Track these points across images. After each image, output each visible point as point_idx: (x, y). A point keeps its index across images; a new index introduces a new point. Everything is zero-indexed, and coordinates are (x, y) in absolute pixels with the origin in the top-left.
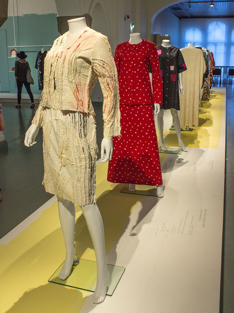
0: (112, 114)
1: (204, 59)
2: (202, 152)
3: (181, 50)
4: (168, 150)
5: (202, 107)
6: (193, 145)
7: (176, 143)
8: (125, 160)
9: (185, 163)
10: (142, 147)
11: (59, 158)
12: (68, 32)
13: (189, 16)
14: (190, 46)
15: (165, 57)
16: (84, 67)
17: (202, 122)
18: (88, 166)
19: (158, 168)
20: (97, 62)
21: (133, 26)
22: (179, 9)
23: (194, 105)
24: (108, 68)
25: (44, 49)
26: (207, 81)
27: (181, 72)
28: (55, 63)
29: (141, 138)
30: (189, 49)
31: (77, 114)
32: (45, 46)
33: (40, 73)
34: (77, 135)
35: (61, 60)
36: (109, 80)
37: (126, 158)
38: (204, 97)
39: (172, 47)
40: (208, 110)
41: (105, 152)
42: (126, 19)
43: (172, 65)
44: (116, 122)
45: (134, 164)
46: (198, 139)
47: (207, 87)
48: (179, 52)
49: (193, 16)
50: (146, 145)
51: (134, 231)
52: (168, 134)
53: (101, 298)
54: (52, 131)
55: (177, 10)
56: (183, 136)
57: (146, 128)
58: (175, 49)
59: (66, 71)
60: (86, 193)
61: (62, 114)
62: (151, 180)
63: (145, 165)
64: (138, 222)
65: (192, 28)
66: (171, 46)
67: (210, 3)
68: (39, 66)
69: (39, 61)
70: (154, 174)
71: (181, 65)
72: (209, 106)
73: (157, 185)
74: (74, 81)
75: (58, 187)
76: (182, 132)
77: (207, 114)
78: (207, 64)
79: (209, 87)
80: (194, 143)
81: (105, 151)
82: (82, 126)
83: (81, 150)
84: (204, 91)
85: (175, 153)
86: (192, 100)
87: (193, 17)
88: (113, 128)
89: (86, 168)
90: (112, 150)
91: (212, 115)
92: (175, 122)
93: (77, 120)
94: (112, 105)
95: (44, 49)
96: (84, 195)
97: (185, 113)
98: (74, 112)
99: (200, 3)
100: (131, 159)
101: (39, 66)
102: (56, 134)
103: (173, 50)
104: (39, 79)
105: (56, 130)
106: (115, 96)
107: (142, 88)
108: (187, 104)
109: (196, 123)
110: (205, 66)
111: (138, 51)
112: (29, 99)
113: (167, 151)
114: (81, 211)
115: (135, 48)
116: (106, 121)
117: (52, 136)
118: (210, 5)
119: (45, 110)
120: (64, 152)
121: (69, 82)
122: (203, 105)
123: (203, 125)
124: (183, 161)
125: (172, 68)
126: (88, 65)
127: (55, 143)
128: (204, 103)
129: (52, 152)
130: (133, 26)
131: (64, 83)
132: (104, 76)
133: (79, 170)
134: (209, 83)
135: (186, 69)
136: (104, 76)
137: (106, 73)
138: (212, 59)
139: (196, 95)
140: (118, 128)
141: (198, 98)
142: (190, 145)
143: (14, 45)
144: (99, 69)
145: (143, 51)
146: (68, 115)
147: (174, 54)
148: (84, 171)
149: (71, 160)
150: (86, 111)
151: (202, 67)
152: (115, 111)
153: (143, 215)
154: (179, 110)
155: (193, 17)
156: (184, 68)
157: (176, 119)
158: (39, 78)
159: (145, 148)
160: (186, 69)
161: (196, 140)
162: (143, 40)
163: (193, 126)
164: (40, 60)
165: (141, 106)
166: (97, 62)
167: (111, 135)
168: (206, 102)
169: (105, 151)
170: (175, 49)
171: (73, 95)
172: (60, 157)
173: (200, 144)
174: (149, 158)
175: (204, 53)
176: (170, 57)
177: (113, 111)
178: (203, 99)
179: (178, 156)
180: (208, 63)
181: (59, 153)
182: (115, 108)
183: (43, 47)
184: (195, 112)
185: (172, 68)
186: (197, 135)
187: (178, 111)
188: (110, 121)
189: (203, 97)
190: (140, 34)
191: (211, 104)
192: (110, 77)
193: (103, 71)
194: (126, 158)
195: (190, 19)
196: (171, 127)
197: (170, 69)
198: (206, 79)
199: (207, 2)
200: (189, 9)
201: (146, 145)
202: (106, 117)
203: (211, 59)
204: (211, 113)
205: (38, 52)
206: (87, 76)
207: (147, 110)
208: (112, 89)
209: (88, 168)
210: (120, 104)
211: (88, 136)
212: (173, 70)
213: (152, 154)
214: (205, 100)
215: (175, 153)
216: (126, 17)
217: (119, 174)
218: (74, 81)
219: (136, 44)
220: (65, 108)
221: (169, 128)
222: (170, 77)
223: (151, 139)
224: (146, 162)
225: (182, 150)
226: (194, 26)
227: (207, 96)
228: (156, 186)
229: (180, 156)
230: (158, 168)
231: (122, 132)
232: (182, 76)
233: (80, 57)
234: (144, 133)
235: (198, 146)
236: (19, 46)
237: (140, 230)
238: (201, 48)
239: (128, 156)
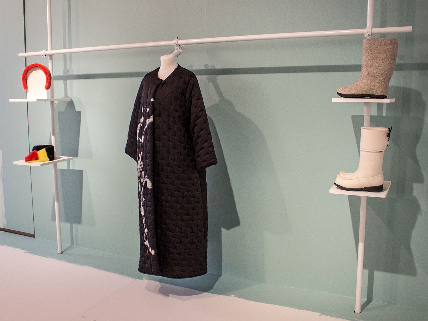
25: (171, 56)
32: (181, 42)
33: (149, 185)
68: (142, 147)
69: (145, 122)
95: (171, 56)
101: (142, 147)
104: (141, 217)
112: (198, 75)
119: (212, 65)
143: (364, 26)
158: (143, 213)
164: (147, 116)
183: (167, 50)
205: (141, 79)
236: (70, 47)
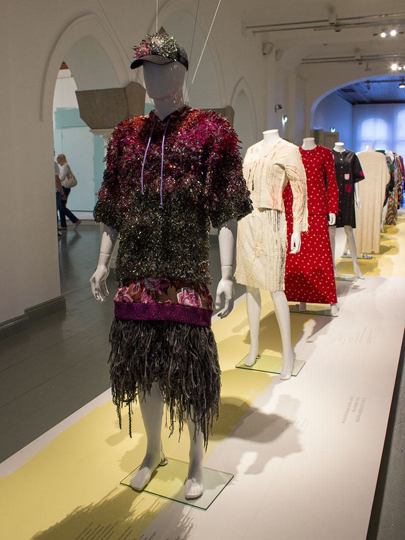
0: (301, 212)
1: (388, 165)
2: (384, 280)
3: (357, 154)
4: (341, 277)
5: (385, 232)
6: (371, 273)
7: (352, 271)
8: (296, 275)
9: (362, 290)
10: (316, 260)
11: (254, 250)
12: (262, 141)
13: (367, 101)
14: (369, 149)
15: (338, 164)
16: (279, 172)
17: (384, 250)
18: (280, 257)
19: (332, 284)
20: (290, 168)
21: (286, 119)
22: (352, 91)
23: (373, 224)
24: (299, 173)
26: (393, 196)
27: (358, 181)
28: (254, 169)
29: (314, 251)
30: (367, 154)
31: (272, 211)
34: (272, 229)
35: (260, 166)
36: (300, 183)
37: (297, 273)
38: (388, 220)
39: (347, 152)
40: (393, 236)
41: (295, 246)
42: (277, 110)
43: (347, 173)
44: (304, 219)
45: (306, 280)
46: (379, 268)
47: (394, 206)
48: (355, 157)
49: (374, 101)
50: (320, 258)
51: (310, 339)
52: (340, 263)
53: (287, 376)
54: (248, 227)
55: (348, 93)
56: (359, 264)
57: (321, 239)
58: (350, 154)
59: (264, 174)
60: (277, 280)
61: (259, 211)
62: (325, 297)
63: (318, 280)
64: (313, 334)
65: (372, 119)
66: (345, 150)
67: (400, 83)
70: (328, 291)
71: (357, 173)
72: (396, 232)
73: (331, 303)
74: (271, 184)
75: (250, 277)
76: (358, 260)
77: (392, 241)
78: (392, 173)
79: (397, 206)
80: (374, 271)
81: (295, 244)
82: (276, 221)
83: (275, 242)
84: (388, 212)
85: (351, 281)
86: (371, 219)
87: (374, 102)
88: (302, 224)
89: (278, 258)
90: (301, 243)
91: (398, 242)
92: (350, 243)
93: (272, 216)
94: (301, 205)
96: (275, 282)
97: (362, 235)
98: (270, 209)
99: (384, 83)
100: (302, 275)
102: (251, 228)
103: (348, 156)
105: (252, 225)
106: (304, 196)
107: (317, 197)
108: (365, 224)
109: (377, 250)
110: (389, 176)
111: (312, 158)
113: (339, 278)
114: (248, 326)
115: (309, 154)
116: (296, 218)
117: (248, 231)
118: (400, 85)
120: (258, 245)
121: (267, 184)
122: (388, 230)
123: (387, 252)
124: (359, 288)
125: (347, 177)
126: (282, 170)
127: (250, 238)
128: (389, 228)
129: (246, 245)
130: (286, 119)
131: (262, 185)
132: (295, 180)
133: (272, 259)
134: (396, 200)
135: (363, 178)
136: (295, 180)
137: (298, 178)
138: (401, 165)
139: (376, 213)
140: (306, 224)
141: (379, 221)
142: (368, 273)
144: (291, 174)
145: (318, 158)
146: (264, 212)
147: (349, 160)
148: (276, 260)
149: (266, 251)
150: (280, 209)
151: (384, 176)
152: (304, 209)
153: (316, 329)
154: (354, 227)
155: (374, 102)
156: (361, 177)
157: (351, 242)
159: (318, 262)
160: (363, 178)
161: (376, 268)
162: (318, 146)
163: (373, 253)
165: (315, 216)
166: (290, 168)
167: (300, 230)
168: (392, 227)
169: (295, 244)
170: (350, 154)
171: (270, 195)
172: (255, 250)
173: (381, 273)
174: (323, 273)
175: (388, 159)
176: (344, 164)
177: (302, 209)
178: (387, 223)
179: (353, 283)
180: (393, 171)
181: (253, 246)
182: (304, 207)
184: (375, 234)
185: (347, 177)
186: (377, 263)
187: (354, 229)
188: (299, 218)
189: (386, 219)
190: (314, 139)
191: (399, 230)
192: (301, 180)
193: (295, 176)
194: (297, 273)
195: (368, 105)
196: (342, 254)
197: (344, 178)
198: (390, 193)
199: (395, 81)
200: (368, 91)
201: (320, 258)
202: (295, 214)
203: (400, 166)
204: (398, 240)
206: (280, 180)
207: (321, 220)
208: (301, 191)
209: (279, 258)
210: (308, 204)
211: (280, 231)
212: (348, 178)
213: (326, 268)
214: (390, 224)
215: (351, 281)
216: (277, 107)
217: (313, 256)
218: (271, 184)
219: (310, 149)
220: (262, 206)
221: (341, 256)
222: (344, 188)
223: (325, 252)
224: (320, 277)
225: (359, 278)
226: (375, 115)
227: (393, 218)
228: (329, 304)
229: (355, 283)
230: (332, 284)
231: (309, 229)
232: (358, 186)
233: (276, 164)
234: (317, 246)
235: (379, 274)
237: (316, 339)
238: (383, 152)
239: (299, 270)
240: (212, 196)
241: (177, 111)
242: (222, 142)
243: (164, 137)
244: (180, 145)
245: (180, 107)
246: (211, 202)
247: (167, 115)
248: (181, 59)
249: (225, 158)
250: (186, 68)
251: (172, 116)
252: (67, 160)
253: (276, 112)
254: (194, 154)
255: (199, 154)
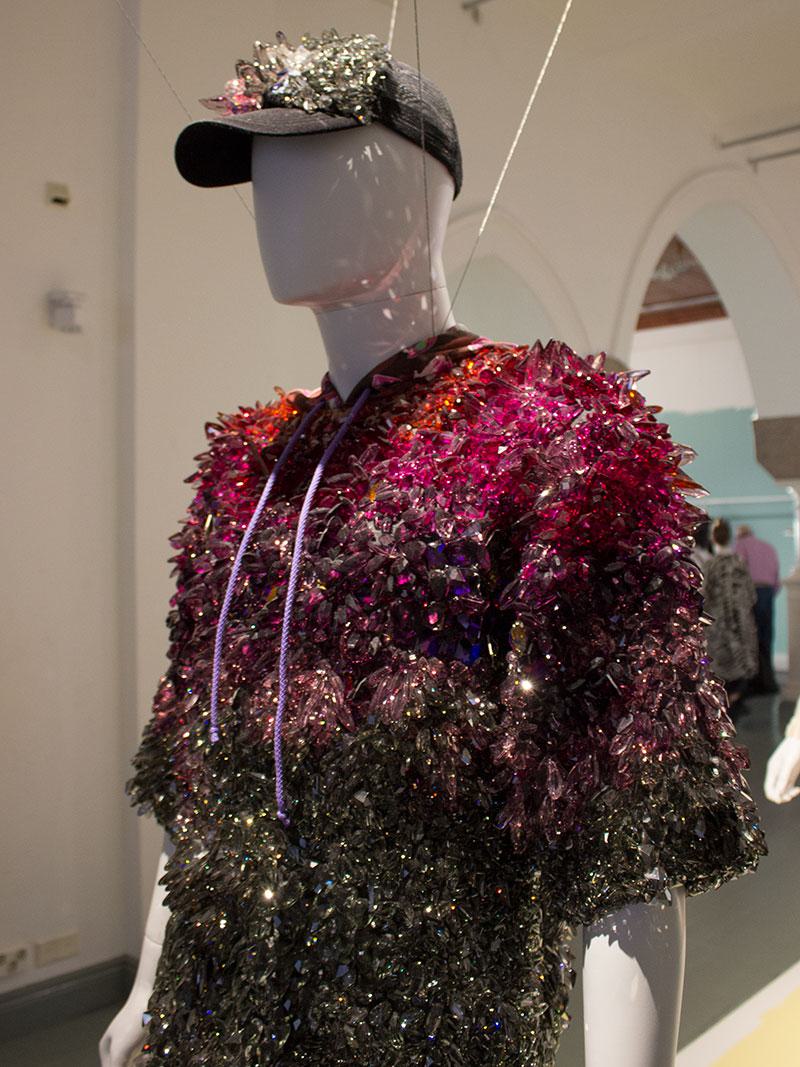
240: (535, 777)
241: (401, 353)
242: (582, 488)
243: (318, 471)
244: (387, 508)
245: (414, 340)
246: (533, 803)
247: (364, 375)
248: (399, 122)
249: (600, 577)
250: (437, 169)
251: (376, 381)
252: (643, 395)
253: (276, 388)
254: (448, 554)
255: (470, 547)
